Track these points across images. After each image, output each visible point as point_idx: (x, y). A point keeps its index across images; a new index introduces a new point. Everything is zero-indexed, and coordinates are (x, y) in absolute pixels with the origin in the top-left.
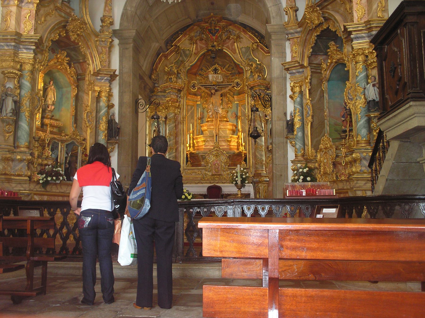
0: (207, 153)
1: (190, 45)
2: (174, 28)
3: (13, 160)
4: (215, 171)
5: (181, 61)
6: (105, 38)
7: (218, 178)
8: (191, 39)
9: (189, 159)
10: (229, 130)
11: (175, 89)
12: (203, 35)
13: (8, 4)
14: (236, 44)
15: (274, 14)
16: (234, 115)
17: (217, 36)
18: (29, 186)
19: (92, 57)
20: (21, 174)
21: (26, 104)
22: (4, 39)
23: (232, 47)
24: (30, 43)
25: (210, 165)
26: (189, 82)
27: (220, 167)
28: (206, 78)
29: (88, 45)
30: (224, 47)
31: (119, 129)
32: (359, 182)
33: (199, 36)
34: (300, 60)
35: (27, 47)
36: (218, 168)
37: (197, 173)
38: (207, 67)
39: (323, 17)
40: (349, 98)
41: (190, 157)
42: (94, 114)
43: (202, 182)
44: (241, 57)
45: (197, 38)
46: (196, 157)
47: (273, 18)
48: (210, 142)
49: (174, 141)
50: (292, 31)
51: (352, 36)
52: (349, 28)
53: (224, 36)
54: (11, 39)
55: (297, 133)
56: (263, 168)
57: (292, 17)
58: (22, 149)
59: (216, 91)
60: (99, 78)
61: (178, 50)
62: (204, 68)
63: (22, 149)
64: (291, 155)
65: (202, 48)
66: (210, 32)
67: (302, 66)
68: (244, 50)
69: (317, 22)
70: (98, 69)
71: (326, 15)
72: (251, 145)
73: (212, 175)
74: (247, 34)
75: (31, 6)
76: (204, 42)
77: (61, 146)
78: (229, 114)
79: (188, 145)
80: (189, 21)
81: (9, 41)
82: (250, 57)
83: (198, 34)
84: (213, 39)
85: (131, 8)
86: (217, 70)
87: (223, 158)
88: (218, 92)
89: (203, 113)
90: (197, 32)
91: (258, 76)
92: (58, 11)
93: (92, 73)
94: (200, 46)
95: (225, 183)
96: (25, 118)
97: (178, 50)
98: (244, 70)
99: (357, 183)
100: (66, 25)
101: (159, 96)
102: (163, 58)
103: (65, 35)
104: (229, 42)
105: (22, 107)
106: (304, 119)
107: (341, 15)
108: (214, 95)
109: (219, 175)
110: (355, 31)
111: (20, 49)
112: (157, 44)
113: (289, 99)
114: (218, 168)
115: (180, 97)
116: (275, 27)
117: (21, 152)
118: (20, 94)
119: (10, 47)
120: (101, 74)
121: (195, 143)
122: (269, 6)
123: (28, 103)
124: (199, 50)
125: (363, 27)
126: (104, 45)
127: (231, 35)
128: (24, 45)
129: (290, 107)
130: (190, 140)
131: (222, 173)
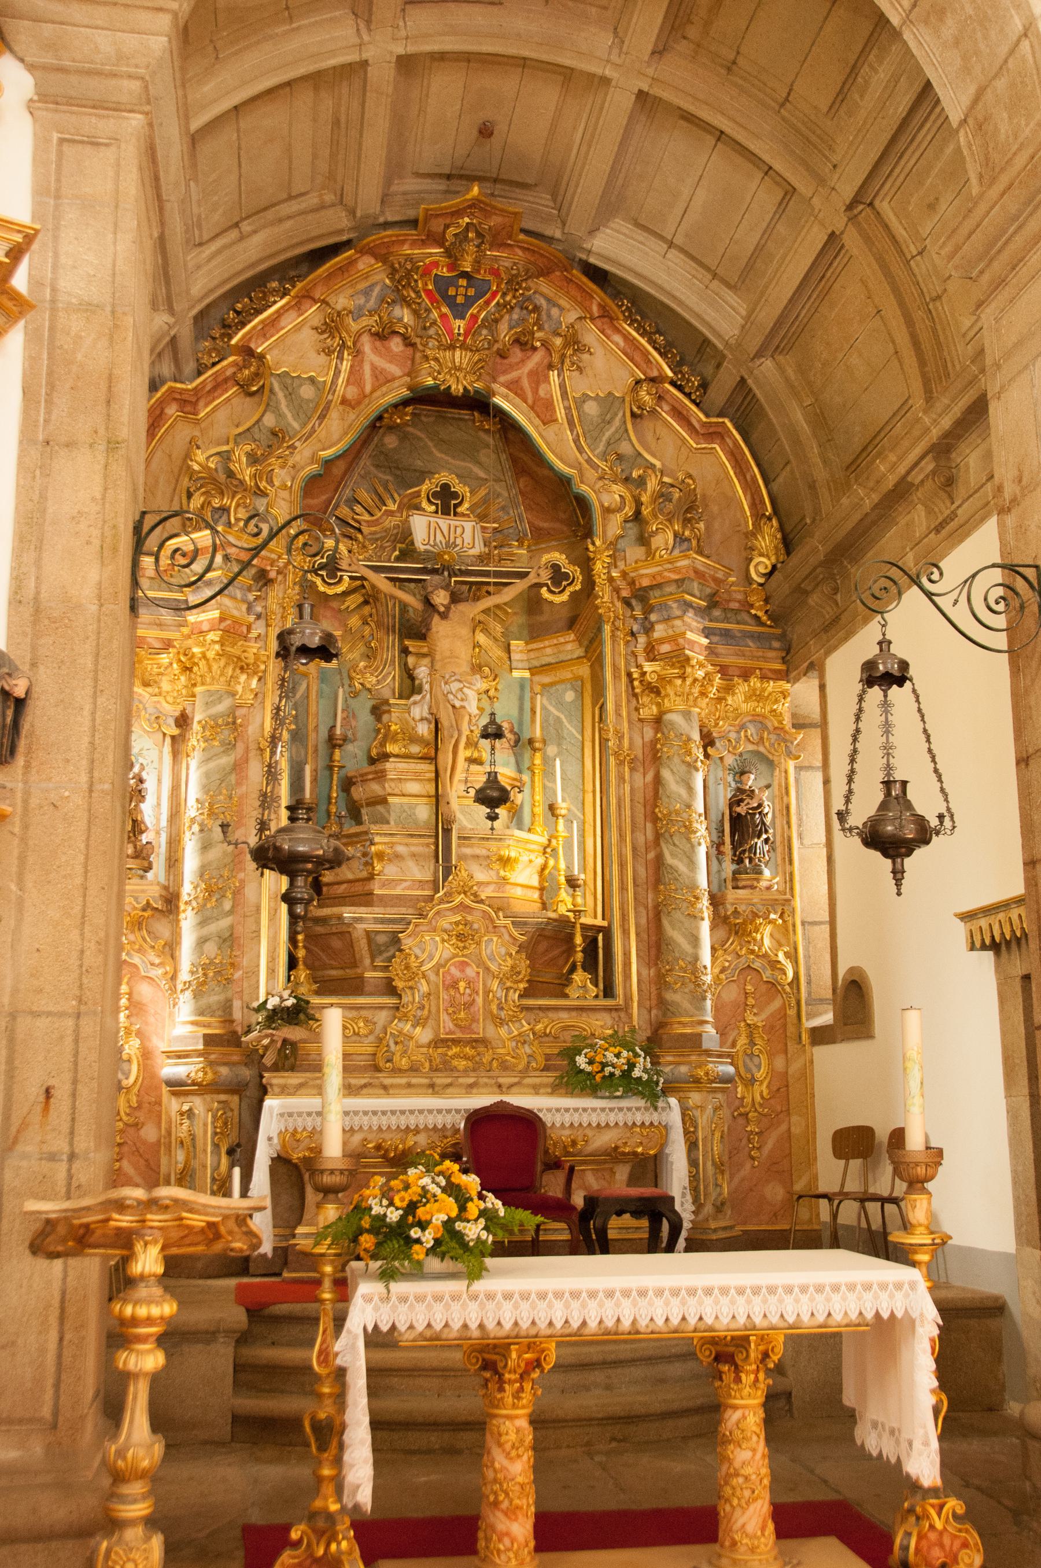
1: (323, 358)
2: (255, 249)
7: (466, 1057)
8: (331, 326)
14: (554, 375)
17: (474, 317)
23: (535, 391)
25: (424, 987)
27: (480, 1000)
30: (496, 387)
31: (20, 704)
36: (469, 1005)
43: (387, 1081)
44: (576, 441)
45: (366, 321)
46: (336, 943)
48: (411, 864)
53: (503, 327)
56: (701, 1009)
59: (455, 598)
61: (257, 375)
65: (382, 379)
66: (442, 292)
68: (591, 408)
73: (438, 1042)
74: (618, 330)
76: (396, 345)
80: (336, 223)
82: (625, 448)
83: (372, 303)
84: (450, 331)
86: (455, 495)
87: (499, 951)
88: (462, 607)
90: (367, 293)
91: (676, 536)
94: (374, 368)
95: (365, 1086)
108: (444, 616)
124: (368, 388)
127: (541, 328)
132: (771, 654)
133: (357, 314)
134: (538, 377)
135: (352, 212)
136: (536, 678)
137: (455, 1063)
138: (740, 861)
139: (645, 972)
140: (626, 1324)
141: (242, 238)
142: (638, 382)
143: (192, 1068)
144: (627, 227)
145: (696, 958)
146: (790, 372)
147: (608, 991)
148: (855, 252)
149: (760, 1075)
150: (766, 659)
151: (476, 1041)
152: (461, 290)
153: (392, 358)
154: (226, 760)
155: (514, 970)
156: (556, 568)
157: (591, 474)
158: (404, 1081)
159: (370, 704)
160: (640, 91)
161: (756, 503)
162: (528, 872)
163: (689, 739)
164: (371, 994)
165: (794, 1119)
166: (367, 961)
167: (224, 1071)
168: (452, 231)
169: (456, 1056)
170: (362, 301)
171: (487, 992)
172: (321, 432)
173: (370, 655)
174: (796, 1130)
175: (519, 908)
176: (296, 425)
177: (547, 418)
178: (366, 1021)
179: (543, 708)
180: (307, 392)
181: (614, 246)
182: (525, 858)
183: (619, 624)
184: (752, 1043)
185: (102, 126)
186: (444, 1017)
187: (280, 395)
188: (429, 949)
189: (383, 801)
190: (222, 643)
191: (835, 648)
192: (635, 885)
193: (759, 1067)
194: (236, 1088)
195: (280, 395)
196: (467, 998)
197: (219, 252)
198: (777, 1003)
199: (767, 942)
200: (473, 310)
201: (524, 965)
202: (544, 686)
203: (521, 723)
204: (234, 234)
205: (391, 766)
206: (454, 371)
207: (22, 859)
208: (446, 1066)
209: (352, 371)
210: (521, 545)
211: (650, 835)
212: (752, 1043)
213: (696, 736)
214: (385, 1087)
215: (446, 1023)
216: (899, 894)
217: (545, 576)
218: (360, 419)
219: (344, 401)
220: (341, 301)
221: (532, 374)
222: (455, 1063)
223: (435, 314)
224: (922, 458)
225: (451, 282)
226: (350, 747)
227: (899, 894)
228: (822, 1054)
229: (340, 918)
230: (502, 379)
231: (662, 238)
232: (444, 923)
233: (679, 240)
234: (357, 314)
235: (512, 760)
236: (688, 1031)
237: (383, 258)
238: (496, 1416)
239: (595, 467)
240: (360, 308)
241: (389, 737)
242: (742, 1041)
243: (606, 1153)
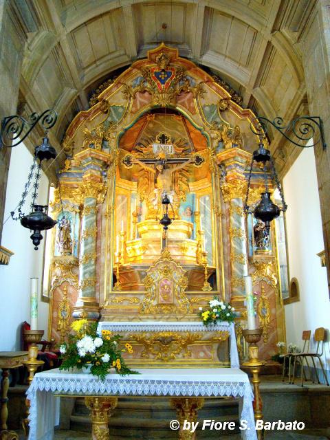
0: (148, 267)
4: (164, 298)
5: (111, 123)
7: (167, 309)
9: (118, 277)
11: (98, 160)
14: (195, 100)
16: (188, 211)
25: (154, 288)
26: (122, 154)
27: (172, 291)
33: (140, 85)
37: (130, 300)
41: (120, 274)
45: (136, 88)
46: (130, 275)
49: (94, 245)
65: (143, 105)
68: (207, 109)
73: (158, 305)
74: (213, 85)
76: (146, 94)
78: (182, 210)
79: (117, 254)
82: (218, 120)
87: (178, 276)
88: (167, 170)
89: (141, 207)
94: (140, 102)
95: (134, 318)
101: (72, 174)
102: (82, 119)
104: (185, 97)
109: (171, 305)
112: (73, 91)
114: (168, 293)
115: (106, 176)
124: (138, 108)
130: (120, 247)
133: (134, 86)
134: (190, 101)
137: (164, 311)
138: (258, 246)
140: (178, 394)
141: (97, 66)
142: (221, 100)
143: (80, 312)
144: (212, 53)
146: (265, 91)
148: (277, 48)
149: (267, 315)
151: (171, 304)
152: (163, 76)
153: (145, 98)
155: (183, 282)
157: (208, 128)
158: (145, 317)
160: (206, 7)
163: (239, 207)
164: (141, 290)
165: (279, 329)
166: (139, 280)
167: (90, 313)
168: (157, 58)
171: (174, 289)
172: (124, 121)
174: (279, 333)
175: (188, 263)
177: (193, 113)
180: (121, 110)
181: (209, 59)
182: (190, 248)
183: (217, 173)
184: (264, 305)
186: (160, 297)
187: (113, 112)
191: (284, 175)
192: (224, 254)
193: (266, 312)
195: (113, 112)
196: (167, 291)
197: (90, 70)
198: (272, 292)
201: (186, 280)
203: (193, 208)
204: (94, 65)
206: (162, 100)
208: (161, 312)
209: (134, 103)
211: (229, 239)
212: (264, 305)
214: (140, 319)
216: (36, 249)
217: (194, 160)
218: (136, 117)
219: (131, 112)
220: (129, 83)
221: (188, 100)
222: (164, 311)
223: (156, 84)
224: (300, 105)
225: (160, 73)
227: (36, 249)
228: (287, 307)
230: (179, 102)
231: (223, 55)
233: (228, 54)
234: (134, 86)
236: (240, 300)
237: (140, 69)
238: (94, 424)
243: (209, 340)
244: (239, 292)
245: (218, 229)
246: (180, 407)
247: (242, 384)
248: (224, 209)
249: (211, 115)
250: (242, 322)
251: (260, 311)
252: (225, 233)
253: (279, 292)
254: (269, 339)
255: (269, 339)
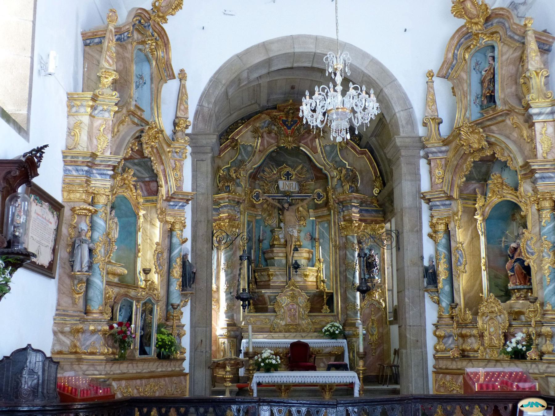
3: (83, 332)
4: (291, 320)
5: (241, 161)
6: (180, 148)
7: (294, 329)
8: (255, 131)
10: (305, 258)
12: (273, 127)
13: (76, 112)
14: (317, 140)
15: (404, 122)
17: (293, 129)
18: (105, 368)
19: (165, 176)
20: (95, 351)
21: (100, 251)
22: (72, 162)
23: (312, 145)
24: (106, 167)
25: (283, 311)
27: (297, 314)
28: (270, 182)
29: (161, 159)
31: (195, 273)
32: (551, 365)
33: (267, 127)
34: (447, 190)
35: (102, 172)
36: (294, 315)
38: (271, 167)
39: (487, 141)
40: (528, 252)
42: (166, 255)
44: (324, 158)
45: (265, 129)
47: (403, 127)
48: (280, 277)
50: (434, 150)
51: (537, 175)
52: (533, 165)
53: (302, 129)
54: (83, 162)
55: (444, 286)
56: (357, 316)
57: (433, 131)
58: (95, 315)
60: (172, 203)
62: (266, 169)
63: (95, 315)
64: (431, 314)
65: (269, 144)
66: (284, 123)
67: (450, 198)
68: (328, 148)
69: (476, 146)
70: (173, 192)
71: (493, 140)
72: (339, 282)
73: (286, 325)
75: (106, 115)
77: (136, 306)
81: (79, 163)
82: (337, 159)
83: (266, 125)
84: (287, 133)
85: (208, 104)
87: (303, 300)
90: (265, 122)
91: (350, 186)
92: (131, 116)
93: (164, 198)
96: (99, 272)
97: (236, 145)
98: (329, 176)
99: (548, 367)
100: (141, 136)
103: (137, 148)
104: (308, 137)
105: (95, 256)
106: (453, 268)
107: (515, 142)
108: (287, 210)
110: (540, 169)
111: (92, 175)
113: (425, 238)
116: (407, 140)
117: (94, 320)
118: (91, 237)
119: (81, 173)
120: (175, 198)
121: (257, 277)
122: (396, 111)
123: (102, 250)
124: (266, 147)
125: (552, 165)
126: (178, 158)
128: (97, 169)
129: (428, 249)
131: (300, 322)
132: (380, 215)
133: (262, 128)
135: (259, 105)
136: (317, 220)
139: (343, 305)
145: (355, 302)
147: (332, 311)
149: (375, 333)
150: (378, 217)
153: (272, 138)
154: (230, 253)
155: (307, 306)
156: (319, 194)
159: (270, 229)
161: (375, 173)
162: (312, 277)
165: (385, 345)
166: (269, 303)
169: (291, 328)
170: (263, 124)
173: (270, 215)
176: (247, 158)
178: (268, 319)
179: (319, 228)
180: (249, 149)
184: (373, 324)
185: (203, 157)
186: (288, 318)
187: (242, 150)
188: (284, 300)
189: (273, 258)
190: (229, 222)
194: (236, 337)
195: (242, 150)
198: (380, 314)
199: (377, 297)
200: (293, 127)
202: (319, 222)
203: (313, 233)
205: (275, 250)
207: (195, 299)
210: (312, 181)
212: (373, 324)
213: (356, 242)
215: (289, 320)
221: (310, 140)
223: (283, 128)
226: (265, 242)
229: (261, 292)
230: (302, 142)
232: (288, 294)
234: (262, 128)
235: (310, 244)
239: (329, 165)
240: (263, 126)
241: (275, 239)
242: (371, 324)
244: (352, 315)
245: (336, 260)
246: (323, 389)
247: (354, 377)
248: (341, 242)
249: (331, 155)
250: (354, 339)
251: (370, 330)
252: (342, 264)
253: (386, 314)
254: (377, 353)
255: (377, 353)
